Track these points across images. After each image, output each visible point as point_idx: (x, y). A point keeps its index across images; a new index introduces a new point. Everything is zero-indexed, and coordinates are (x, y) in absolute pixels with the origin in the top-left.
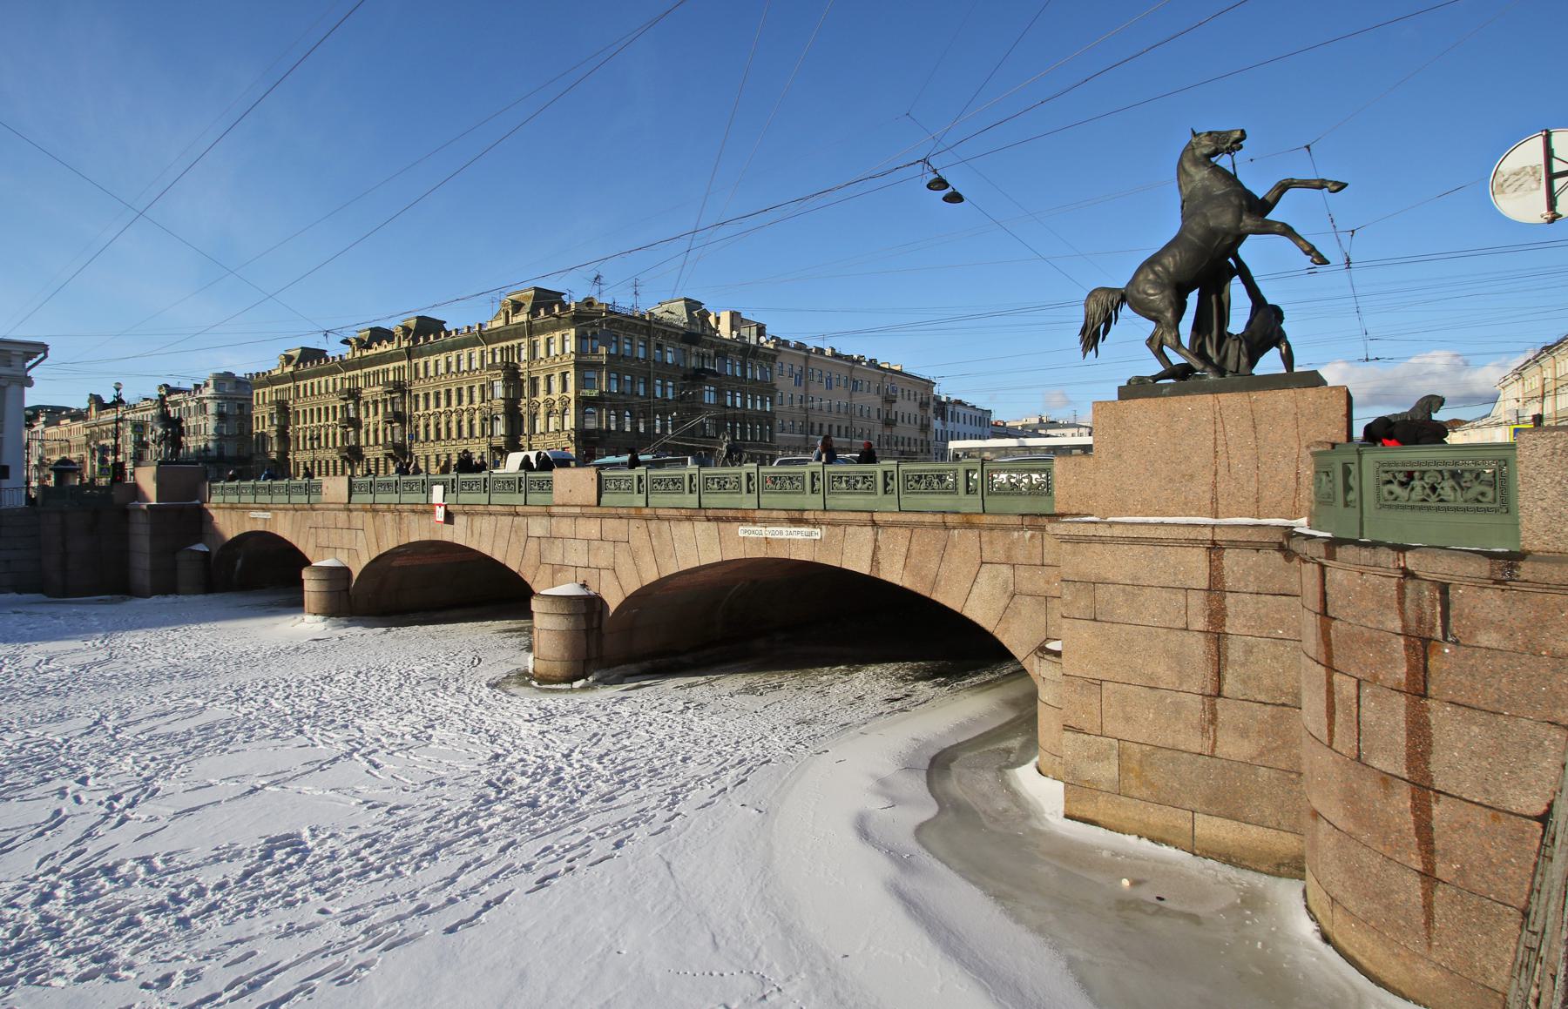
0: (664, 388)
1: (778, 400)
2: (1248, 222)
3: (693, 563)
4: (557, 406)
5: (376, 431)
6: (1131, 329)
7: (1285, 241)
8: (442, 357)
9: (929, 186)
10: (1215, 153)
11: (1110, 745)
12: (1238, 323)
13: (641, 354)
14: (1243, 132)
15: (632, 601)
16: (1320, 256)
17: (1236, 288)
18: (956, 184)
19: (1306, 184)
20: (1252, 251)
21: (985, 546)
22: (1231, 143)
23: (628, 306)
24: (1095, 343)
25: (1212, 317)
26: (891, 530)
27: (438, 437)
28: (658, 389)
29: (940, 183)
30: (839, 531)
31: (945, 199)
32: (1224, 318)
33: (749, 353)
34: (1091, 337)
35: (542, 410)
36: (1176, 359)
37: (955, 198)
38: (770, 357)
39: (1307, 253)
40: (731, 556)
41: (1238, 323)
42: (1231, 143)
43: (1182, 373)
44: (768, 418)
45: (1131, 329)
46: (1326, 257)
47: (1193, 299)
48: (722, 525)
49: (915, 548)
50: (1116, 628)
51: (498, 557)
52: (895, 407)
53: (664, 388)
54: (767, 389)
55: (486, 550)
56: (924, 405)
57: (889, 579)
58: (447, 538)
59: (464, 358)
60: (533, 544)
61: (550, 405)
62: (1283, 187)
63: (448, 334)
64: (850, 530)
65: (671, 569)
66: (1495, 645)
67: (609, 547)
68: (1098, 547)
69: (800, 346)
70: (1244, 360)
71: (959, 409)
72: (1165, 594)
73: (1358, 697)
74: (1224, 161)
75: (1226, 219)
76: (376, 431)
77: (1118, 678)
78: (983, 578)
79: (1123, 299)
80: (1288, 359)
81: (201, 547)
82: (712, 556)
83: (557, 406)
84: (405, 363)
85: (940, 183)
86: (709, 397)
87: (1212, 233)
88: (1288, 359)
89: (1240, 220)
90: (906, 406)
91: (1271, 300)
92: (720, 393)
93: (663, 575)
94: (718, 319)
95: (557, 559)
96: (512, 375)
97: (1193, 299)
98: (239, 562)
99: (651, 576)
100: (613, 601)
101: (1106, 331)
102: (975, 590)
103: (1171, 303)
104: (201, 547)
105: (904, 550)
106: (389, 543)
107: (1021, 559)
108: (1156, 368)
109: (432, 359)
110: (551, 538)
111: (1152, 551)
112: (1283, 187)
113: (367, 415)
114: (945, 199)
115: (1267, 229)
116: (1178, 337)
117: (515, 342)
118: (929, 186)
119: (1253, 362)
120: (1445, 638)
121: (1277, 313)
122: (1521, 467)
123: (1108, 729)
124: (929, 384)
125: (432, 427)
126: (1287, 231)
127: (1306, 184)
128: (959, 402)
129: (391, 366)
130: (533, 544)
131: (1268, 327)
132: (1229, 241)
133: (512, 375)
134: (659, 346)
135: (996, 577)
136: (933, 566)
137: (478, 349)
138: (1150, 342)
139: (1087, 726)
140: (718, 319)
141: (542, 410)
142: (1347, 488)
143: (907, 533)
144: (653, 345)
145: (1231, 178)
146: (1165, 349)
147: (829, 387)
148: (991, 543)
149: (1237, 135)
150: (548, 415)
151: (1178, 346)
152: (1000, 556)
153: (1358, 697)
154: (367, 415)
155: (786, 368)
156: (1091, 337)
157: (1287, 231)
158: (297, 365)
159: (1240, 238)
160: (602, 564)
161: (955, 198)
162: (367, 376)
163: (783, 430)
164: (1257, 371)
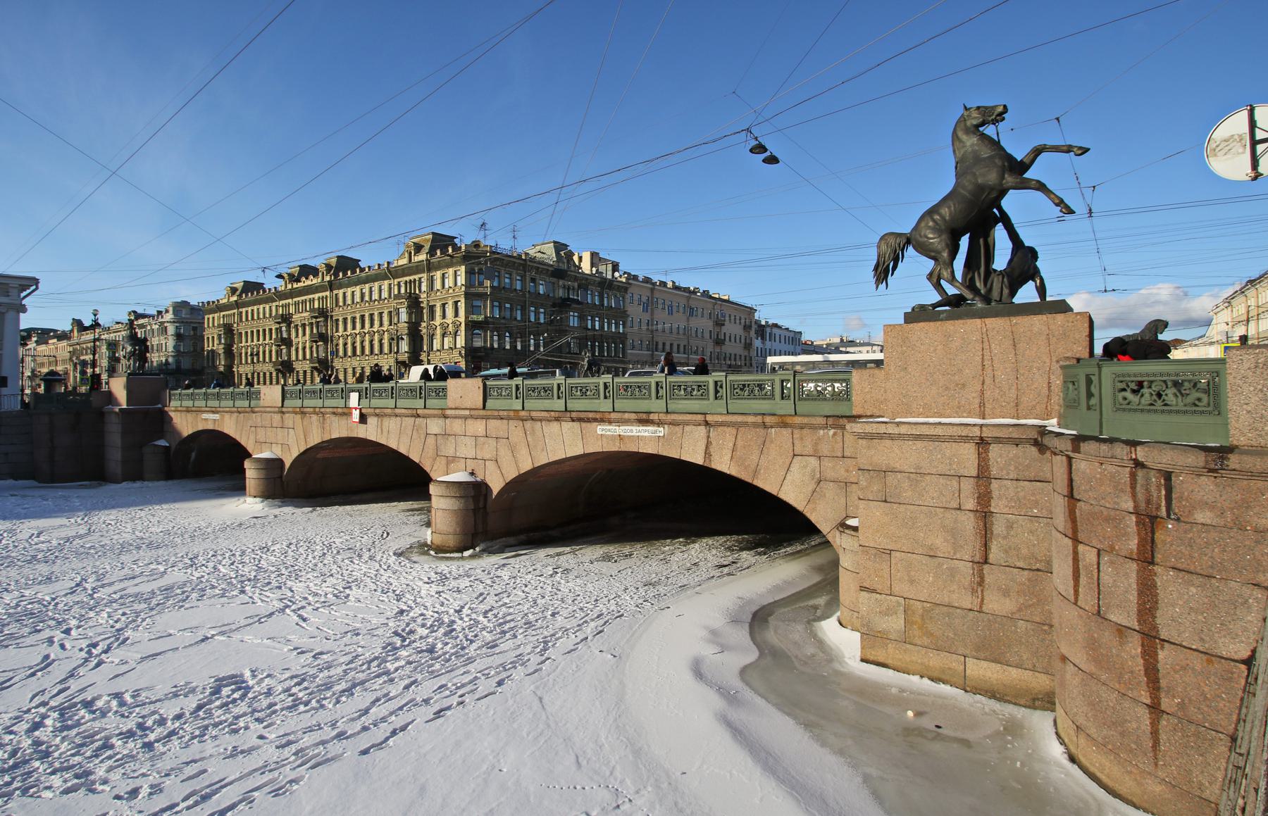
0: (537, 314)
1: (629, 324)
2: (1009, 179)
3: (560, 455)
4: (451, 328)
5: (304, 348)
6: (915, 266)
7: (1039, 195)
8: (357, 289)
9: (751, 151)
10: (983, 124)
11: (898, 602)
12: (1001, 261)
13: (518, 286)
14: (1005, 106)
15: (511, 486)
16: (1067, 207)
17: (1000, 233)
18: (773, 149)
19: (1056, 149)
20: (1013, 203)
21: (796, 442)
22: (996, 116)
23: (508, 247)
24: (886, 278)
25: (980, 256)
26: (720, 429)
27: (354, 353)
28: (532, 315)
29: (760, 148)
30: (678, 429)
31: (764, 161)
32: (989, 257)
33: (606, 285)
34: (883, 273)
35: (439, 331)
36: (951, 290)
37: (772, 160)
38: (623, 289)
39: (1057, 205)
40: (591, 450)
41: (1001, 261)
42: (996, 116)
43: (956, 302)
44: (621, 338)
45: (915, 266)
46: (1073, 208)
47: (964, 242)
48: (584, 425)
49: (740, 443)
50: (902, 508)
51: (403, 450)
52: (724, 329)
53: (537, 314)
54: (620, 315)
55: (393, 445)
56: (747, 328)
57: (719, 468)
58: (361, 435)
59: (376, 289)
60: (431, 440)
61: (444, 327)
62: (1037, 151)
63: (362, 270)
64: (687, 428)
65: (542, 460)
66: (1209, 522)
67: (492, 442)
68: (888, 443)
69: (647, 280)
70: (1006, 291)
71: (775, 330)
72: (942, 480)
73: (1099, 564)
74: (990, 130)
75: (991, 177)
76: (304, 348)
77: (904, 549)
78: (795, 467)
79: (908, 242)
80: (1042, 290)
81: (162, 443)
82: (576, 449)
83: (451, 328)
84: (328, 293)
85: (760, 148)
86: (574, 321)
87: (981, 188)
88: (1042, 290)
89: (1003, 178)
90: (732, 329)
91: (1028, 243)
92: (582, 318)
93: (536, 465)
94: (580, 258)
95: (450, 452)
96: (414, 303)
97: (964, 242)
98: (193, 455)
99: (526, 466)
100: (496, 486)
101: (895, 268)
102: (788, 477)
103: (947, 245)
104: (162, 443)
105: (731, 445)
106: (315, 439)
107: (826, 452)
108: (935, 297)
109: (349, 291)
110: (446, 435)
111: (931, 445)
112: (1037, 151)
113: (297, 336)
114: (764, 161)
115: (1025, 185)
116: (953, 272)
117: (417, 277)
118: (751, 151)
119: (1013, 293)
120: (1169, 516)
121: (1033, 253)
122: (1230, 378)
123: (896, 589)
124: (751, 311)
125: (349, 346)
126: (1041, 187)
127: (1056, 149)
128: (776, 325)
129: (316, 296)
130: (431, 440)
131: (1025, 265)
132: (994, 195)
133: (414, 303)
134: (533, 280)
135: (805, 467)
136: (755, 457)
137: (386, 282)
138: (930, 276)
139: (879, 587)
140: (580, 258)
141: (439, 331)
142: (1090, 395)
143: (734, 431)
144: (528, 279)
145: (996, 144)
146: (942, 282)
147: (671, 313)
148: (802, 439)
149: (1000, 109)
150: (443, 335)
151: (952, 280)
152: (809, 449)
153: (1099, 564)
154: (297, 336)
155: (636, 297)
156: (883, 273)
157: (1041, 187)
158: (240, 296)
159: (1003, 193)
160: (487, 456)
161: (772, 160)
162: (297, 304)
163: (633, 348)
164: (1017, 300)
